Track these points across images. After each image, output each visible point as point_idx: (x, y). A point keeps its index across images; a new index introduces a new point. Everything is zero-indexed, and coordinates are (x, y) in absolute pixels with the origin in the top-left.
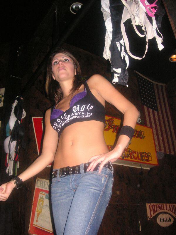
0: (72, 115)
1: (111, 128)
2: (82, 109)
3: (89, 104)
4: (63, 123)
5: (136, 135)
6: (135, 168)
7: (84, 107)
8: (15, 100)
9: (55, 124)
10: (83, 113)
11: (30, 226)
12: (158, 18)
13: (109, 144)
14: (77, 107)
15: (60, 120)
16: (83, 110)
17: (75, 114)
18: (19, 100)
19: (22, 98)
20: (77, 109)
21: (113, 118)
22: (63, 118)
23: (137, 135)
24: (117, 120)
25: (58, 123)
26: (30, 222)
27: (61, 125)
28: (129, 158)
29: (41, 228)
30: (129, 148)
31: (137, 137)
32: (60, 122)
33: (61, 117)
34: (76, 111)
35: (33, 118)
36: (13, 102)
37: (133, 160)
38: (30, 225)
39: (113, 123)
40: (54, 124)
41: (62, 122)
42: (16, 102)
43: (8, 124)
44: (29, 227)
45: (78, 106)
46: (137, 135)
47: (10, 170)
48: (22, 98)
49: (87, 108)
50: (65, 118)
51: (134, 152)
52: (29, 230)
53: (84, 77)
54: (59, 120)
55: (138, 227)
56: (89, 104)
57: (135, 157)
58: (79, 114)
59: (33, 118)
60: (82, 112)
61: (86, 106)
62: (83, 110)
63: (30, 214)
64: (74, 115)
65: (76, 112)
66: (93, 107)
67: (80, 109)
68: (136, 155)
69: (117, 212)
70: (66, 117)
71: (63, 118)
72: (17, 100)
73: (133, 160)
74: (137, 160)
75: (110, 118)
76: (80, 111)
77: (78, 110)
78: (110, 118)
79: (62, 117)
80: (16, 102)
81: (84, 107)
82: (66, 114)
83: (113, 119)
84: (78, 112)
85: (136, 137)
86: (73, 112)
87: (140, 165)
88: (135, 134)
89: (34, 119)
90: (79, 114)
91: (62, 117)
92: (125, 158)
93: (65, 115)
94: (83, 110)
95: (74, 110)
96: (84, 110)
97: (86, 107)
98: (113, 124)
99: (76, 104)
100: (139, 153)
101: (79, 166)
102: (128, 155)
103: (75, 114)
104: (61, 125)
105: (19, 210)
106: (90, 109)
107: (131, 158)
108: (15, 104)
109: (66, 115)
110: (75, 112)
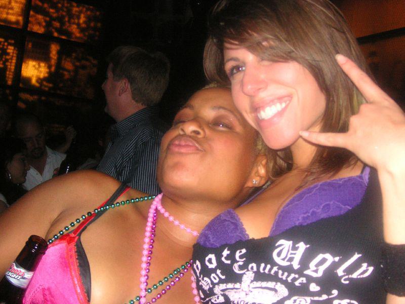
0: (267, 271)
2: (312, 265)
3: (356, 256)
7: (323, 261)
10: (314, 287)
14: (295, 248)
16: (314, 275)
17: (276, 273)
20: (291, 260)
22: (229, 262)
27: (212, 282)
29: (258, 193)
33: (226, 252)
41: (219, 272)
43: (365, 69)
45: (302, 246)
49: (340, 272)
50: (236, 269)
54: (210, 261)
56: (356, 256)
58: (297, 283)
60: (310, 279)
61: (337, 259)
62: (316, 271)
65: (284, 269)
66: (371, 269)
67: (305, 263)
70: (241, 268)
71: (229, 262)
76: (300, 272)
77: (296, 265)
79: (227, 258)
81: (323, 261)
82: (244, 251)
84: (295, 272)
90: (297, 283)
91: (227, 258)
93: (238, 254)
94: (316, 271)
95: (279, 254)
96: (320, 274)
97: (335, 266)
99: (294, 234)
104: (212, 282)
106: (355, 275)
109: (241, 257)
110: (280, 267)
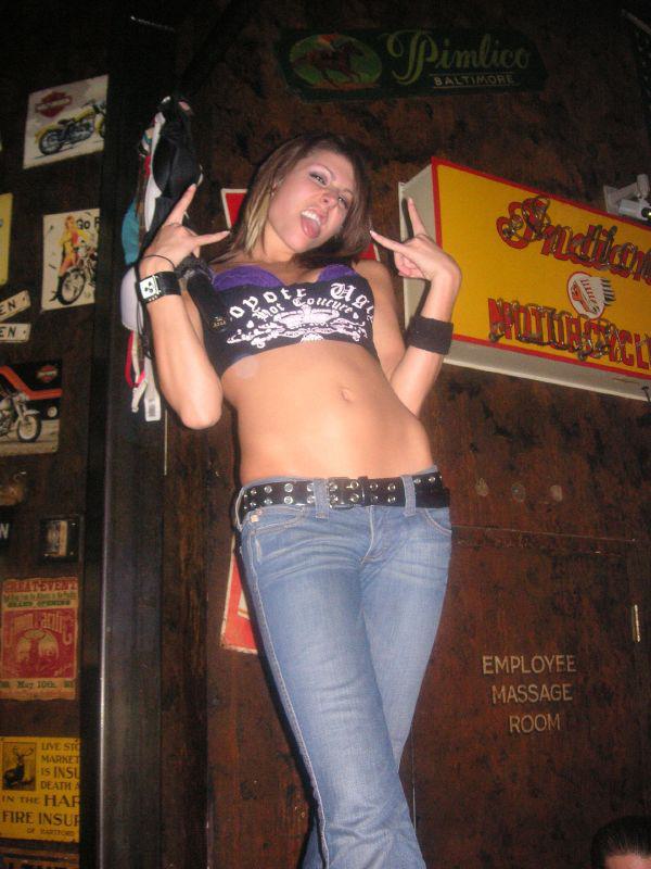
1: (539, 237)
4: (280, 312)
5: (632, 265)
6: (623, 398)
8: (157, 112)
9: (253, 302)
11: (225, 617)
12: (14, 421)
13: (531, 301)
14: (347, 288)
15: (275, 298)
17: (331, 304)
18: (171, 113)
19: (185, 107)
21: (543, 196)
23: (634, 269)
24: (559, 203)
25: (263, 305)
26: (227, 602)
28: (605, 360)
30: (606, 321)
31: (636, 278)
32: (274, 304)
34: (341, 297)
35: (225, 192)
36: (150, 123)
37: (622, 366)
38: (226, 612)
39: (545, 215)
40: (245, 302)
41: (278, 305)
42: (160, 120)
44: (222, 619)
45: (352, 288)
46: (634, 269)
47: (151, 400)
48: (185, 107)
50: (296, 303)
51: (625, 336)
52: (223, 631)
53: (422, 29)
55: (629, 625)
57: (628, 357)
59: (225, 192)
63: (228, 570)
64: (327, 305)
65: (339, 301)
67: (353, 298)
68: (630, 349)
69: (555, 565)
72: (165, 116)
73: (622, 366)
74: (634, 368)
75: (532, 196)
77: (347, 299)
78: (532, 196)
80: (160, 120)
83: (544, 201)
85: (631, 276)
86: (330, 297)
87: (645, 388)
88: (628, 265)
89: (228, 195)
92: (590, 359)
98: (546, 221)
100: (643, 338)
101: (398, 482)
102: (603, 347)
103: (331, 304)
105: (182, 558)
107: (613, 358)
108: (154, 135)
